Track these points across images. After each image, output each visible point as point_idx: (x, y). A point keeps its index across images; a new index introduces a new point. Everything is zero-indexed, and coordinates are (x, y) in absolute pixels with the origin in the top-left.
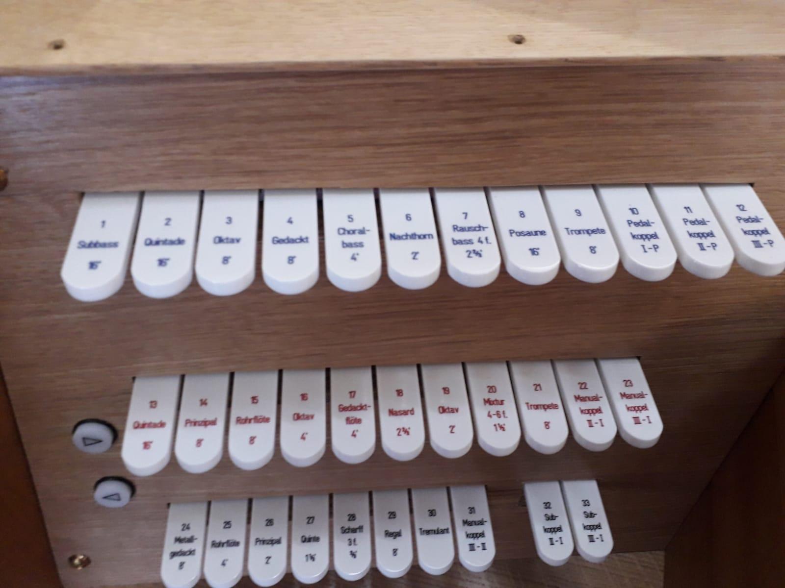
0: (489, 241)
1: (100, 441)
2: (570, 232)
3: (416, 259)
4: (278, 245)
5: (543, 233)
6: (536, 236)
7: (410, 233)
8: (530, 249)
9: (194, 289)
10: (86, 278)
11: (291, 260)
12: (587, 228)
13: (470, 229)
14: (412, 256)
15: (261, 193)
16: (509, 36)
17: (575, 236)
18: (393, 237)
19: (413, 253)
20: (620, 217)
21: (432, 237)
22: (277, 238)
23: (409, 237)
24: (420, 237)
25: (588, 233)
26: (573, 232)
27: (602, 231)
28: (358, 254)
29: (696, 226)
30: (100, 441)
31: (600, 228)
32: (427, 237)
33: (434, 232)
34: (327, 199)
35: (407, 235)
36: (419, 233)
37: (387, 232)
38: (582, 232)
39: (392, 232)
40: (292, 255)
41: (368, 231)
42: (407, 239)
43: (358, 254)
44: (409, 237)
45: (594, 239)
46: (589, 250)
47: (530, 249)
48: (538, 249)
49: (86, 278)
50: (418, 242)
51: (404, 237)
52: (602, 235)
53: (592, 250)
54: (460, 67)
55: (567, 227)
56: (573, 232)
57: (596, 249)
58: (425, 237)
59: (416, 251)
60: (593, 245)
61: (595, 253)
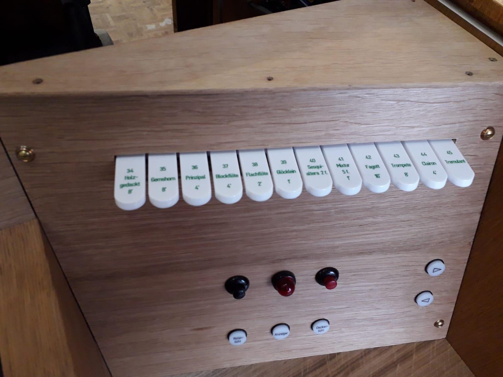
0: (327, 173)
1: (441, 269)
2: (394, 166)
3: (261, 186)
4: (154, 182)
5: (293, 172)
6: (399, 167)
7: (257, 172)
8: (375, 175)
9: (148, 205)
10: (128, 198)
11: (164, 189)
12: (402, 164)
13: (315, 167)
14: (258, 184)
15: (266, 150)
16: (267, 78)
17: (396, 168)
18: (218, 176)
19: (258, 183)
20: (333, 163)
21: (175, 179)
22: (153, 178)
23: (257, 174)
24: (168, 179)
25: (403, 166)
26: (395, 166)
27: (409, 165)
28: (231, 184)
29: (404, 164)
30: (441, 269)
31: (408, 163)
32: (172, 179)
33: (176, 176)
34: (182, 157)
35: (256, 174)
36: (167, 177)
37: (215, 173)
38: (399, 166)
39: (218, 174)
40: (164, 187)
41: (323, 166)
42: (256, 175)
43: (231, 184)
44: (257, 174)
45: (406, 169)
46: (404, 175)
47: (375, 175)
48: (379, 175)
49: (128, 198)
50: (166, 182)
51: (255, 175)
52: (409, 167)
53: (406, 175)
54: (180, 94)
55: (392, 163)
56: (449, 162)
57: (408, 174)
58: (170, 179)
59: (260, 181)
60: (406, 172)
61: (407, 176)
